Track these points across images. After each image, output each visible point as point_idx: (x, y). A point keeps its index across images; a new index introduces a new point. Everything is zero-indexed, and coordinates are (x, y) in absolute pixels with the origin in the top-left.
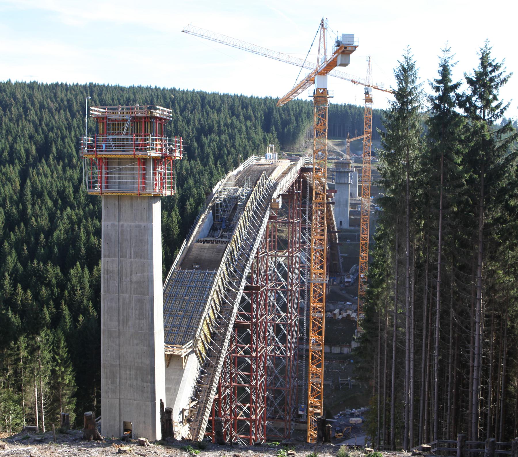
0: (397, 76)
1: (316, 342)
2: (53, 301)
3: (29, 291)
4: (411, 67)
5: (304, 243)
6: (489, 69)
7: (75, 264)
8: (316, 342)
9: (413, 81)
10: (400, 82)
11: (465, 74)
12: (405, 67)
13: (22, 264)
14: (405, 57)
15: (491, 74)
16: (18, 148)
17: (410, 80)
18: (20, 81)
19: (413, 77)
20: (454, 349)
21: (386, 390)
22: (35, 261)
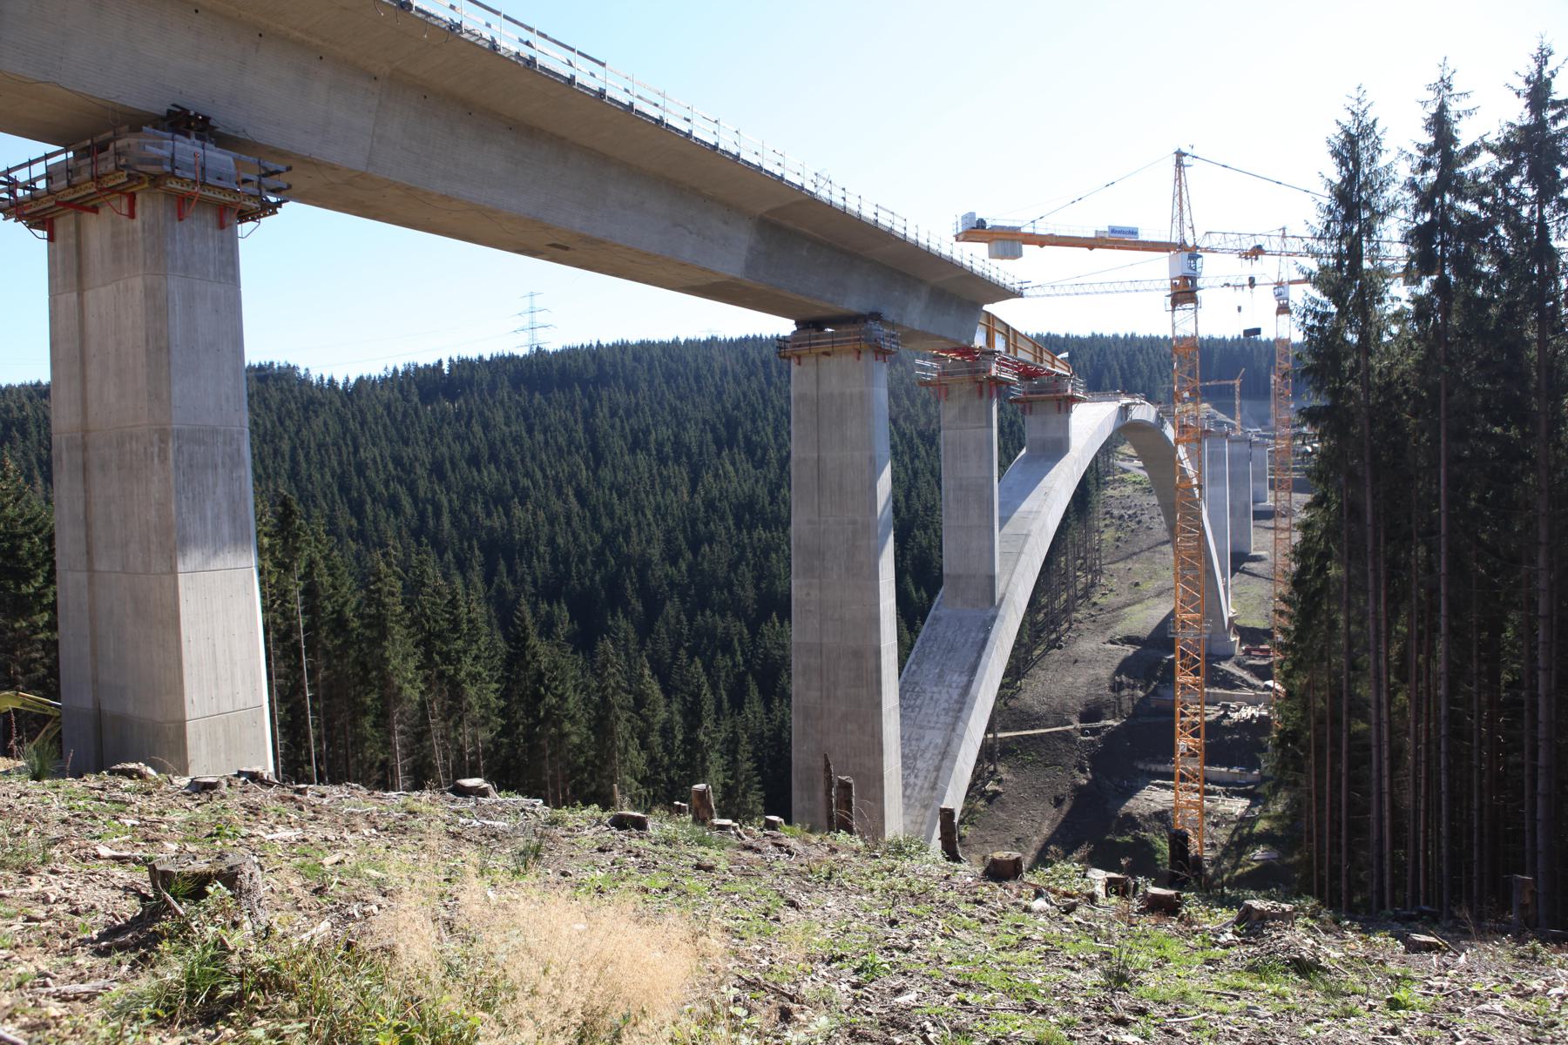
0: (1336, 154)
1: (1189, 750)
2: (754, 677)
3: (696, 659)
4: (1367, 131)
5: (1088, 1020)
6: (1550, 113)
7: (770, 616)
8: (1189, 750)
9: (1373, 159)
10: (1343, 163)
11: (1542, 58)
12: (1353, 131)
13: (750, 632)
14: (1353, 113)
15: (1555, 123)
16: (687, 440)
17: (1365, 156)
18: (692, 337)
19: (1371, 152)
20: (315, 656)
21: (1331, 852)
22: (708, 612)
